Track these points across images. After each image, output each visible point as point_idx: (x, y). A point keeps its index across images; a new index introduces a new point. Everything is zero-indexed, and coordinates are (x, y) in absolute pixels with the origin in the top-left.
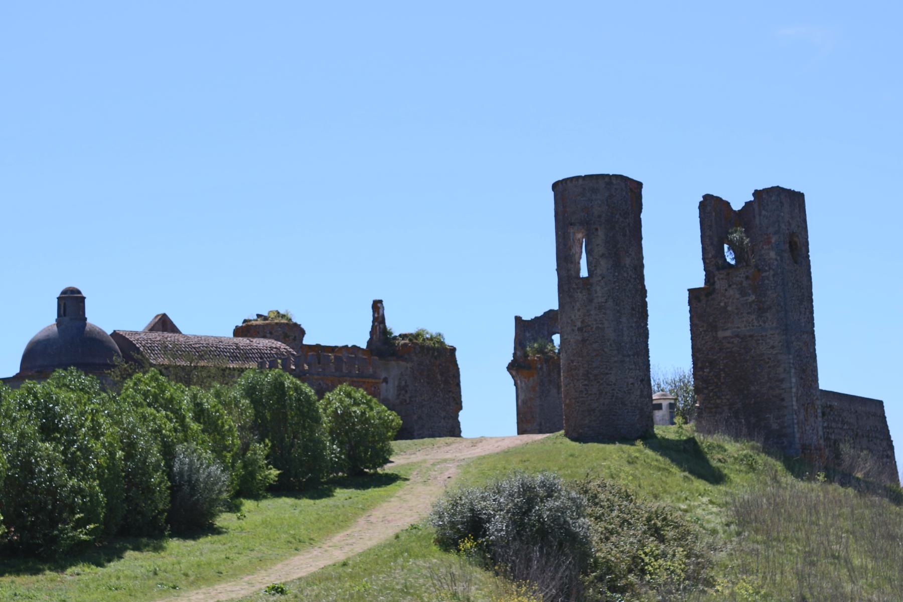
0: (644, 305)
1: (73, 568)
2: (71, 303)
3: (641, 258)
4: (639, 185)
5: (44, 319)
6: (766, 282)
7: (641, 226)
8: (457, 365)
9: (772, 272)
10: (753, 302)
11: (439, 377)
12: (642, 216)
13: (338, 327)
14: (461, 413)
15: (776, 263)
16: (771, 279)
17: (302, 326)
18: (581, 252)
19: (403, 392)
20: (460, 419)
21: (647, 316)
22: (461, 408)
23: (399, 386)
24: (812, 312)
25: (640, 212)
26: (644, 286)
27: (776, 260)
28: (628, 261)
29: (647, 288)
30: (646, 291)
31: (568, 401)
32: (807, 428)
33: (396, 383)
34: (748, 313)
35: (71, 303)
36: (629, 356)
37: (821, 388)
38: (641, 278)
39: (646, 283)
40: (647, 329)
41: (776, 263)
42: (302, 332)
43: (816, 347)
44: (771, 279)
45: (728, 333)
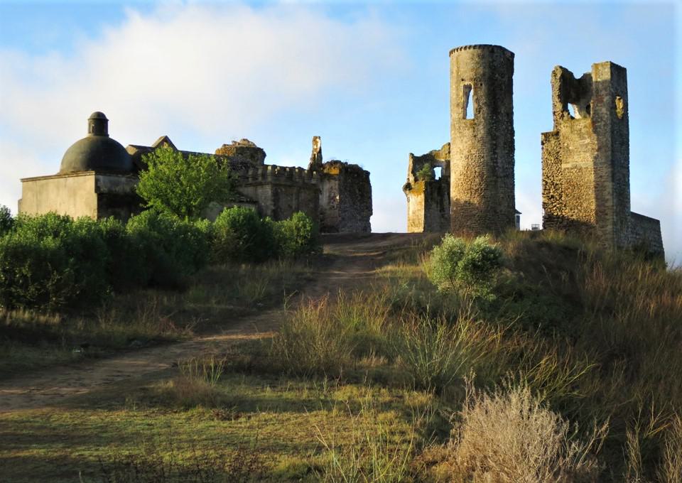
0: (512, 142)
1: (416, 231)
2: (100, 122)
3: (512, 108)
4: (513, 55)
5: (82, 132)
6: (599, 129)
7: (512, 85)
8: (370, 184)
9: (603, 123)
10: (588, 144)
11: (357, 191)
12: (513, 77)
13: (289, 153)
14: (371, 217)
15: (606, 116)
16: (602, 127)
17: (264, 150)
18: (25, 460)
19: (332, 201)
20: (371, 221)
21: (514, 149)
22: (372, 214)
23: (329, 196)
24: (628, 154)
25: (512, 74)
26: (513, 128)
27: (606, 114)
28: (503, 110)
29: (515, 129)
30: (514, 131)
31: (455, 209)
32: (622, 235)
33: (328, 194)
34: (584, 152)
35: (100, 122)
36: (501, 177)
37: (632, 210)
38: (511, 122)
39: (514, 126)
40: (514, 159)
41: (606, 116)
42: (264, 155)
43: (630, 179)
44: (602, 127)
45: (569, 166)
